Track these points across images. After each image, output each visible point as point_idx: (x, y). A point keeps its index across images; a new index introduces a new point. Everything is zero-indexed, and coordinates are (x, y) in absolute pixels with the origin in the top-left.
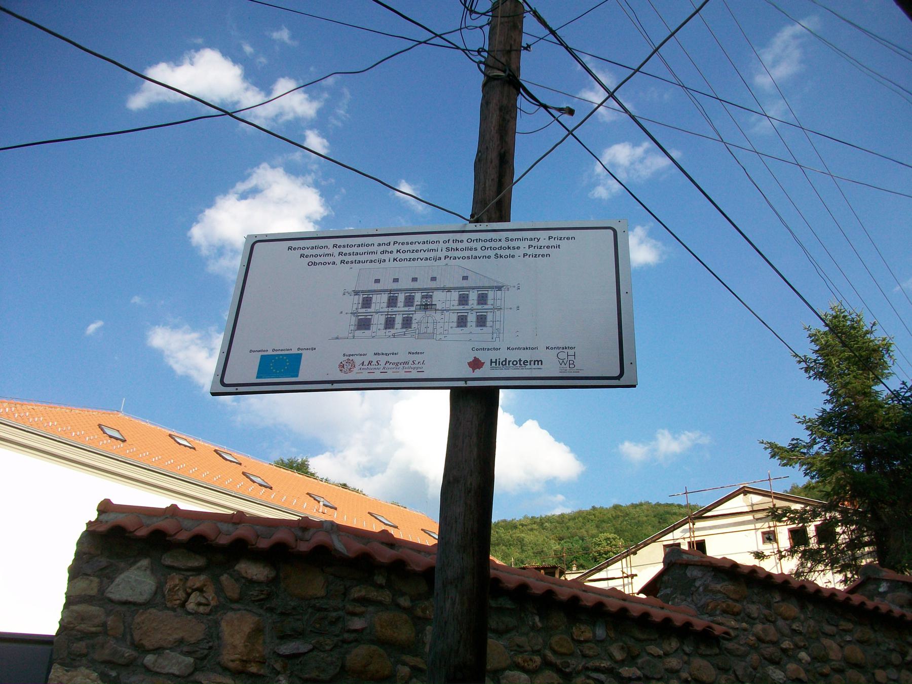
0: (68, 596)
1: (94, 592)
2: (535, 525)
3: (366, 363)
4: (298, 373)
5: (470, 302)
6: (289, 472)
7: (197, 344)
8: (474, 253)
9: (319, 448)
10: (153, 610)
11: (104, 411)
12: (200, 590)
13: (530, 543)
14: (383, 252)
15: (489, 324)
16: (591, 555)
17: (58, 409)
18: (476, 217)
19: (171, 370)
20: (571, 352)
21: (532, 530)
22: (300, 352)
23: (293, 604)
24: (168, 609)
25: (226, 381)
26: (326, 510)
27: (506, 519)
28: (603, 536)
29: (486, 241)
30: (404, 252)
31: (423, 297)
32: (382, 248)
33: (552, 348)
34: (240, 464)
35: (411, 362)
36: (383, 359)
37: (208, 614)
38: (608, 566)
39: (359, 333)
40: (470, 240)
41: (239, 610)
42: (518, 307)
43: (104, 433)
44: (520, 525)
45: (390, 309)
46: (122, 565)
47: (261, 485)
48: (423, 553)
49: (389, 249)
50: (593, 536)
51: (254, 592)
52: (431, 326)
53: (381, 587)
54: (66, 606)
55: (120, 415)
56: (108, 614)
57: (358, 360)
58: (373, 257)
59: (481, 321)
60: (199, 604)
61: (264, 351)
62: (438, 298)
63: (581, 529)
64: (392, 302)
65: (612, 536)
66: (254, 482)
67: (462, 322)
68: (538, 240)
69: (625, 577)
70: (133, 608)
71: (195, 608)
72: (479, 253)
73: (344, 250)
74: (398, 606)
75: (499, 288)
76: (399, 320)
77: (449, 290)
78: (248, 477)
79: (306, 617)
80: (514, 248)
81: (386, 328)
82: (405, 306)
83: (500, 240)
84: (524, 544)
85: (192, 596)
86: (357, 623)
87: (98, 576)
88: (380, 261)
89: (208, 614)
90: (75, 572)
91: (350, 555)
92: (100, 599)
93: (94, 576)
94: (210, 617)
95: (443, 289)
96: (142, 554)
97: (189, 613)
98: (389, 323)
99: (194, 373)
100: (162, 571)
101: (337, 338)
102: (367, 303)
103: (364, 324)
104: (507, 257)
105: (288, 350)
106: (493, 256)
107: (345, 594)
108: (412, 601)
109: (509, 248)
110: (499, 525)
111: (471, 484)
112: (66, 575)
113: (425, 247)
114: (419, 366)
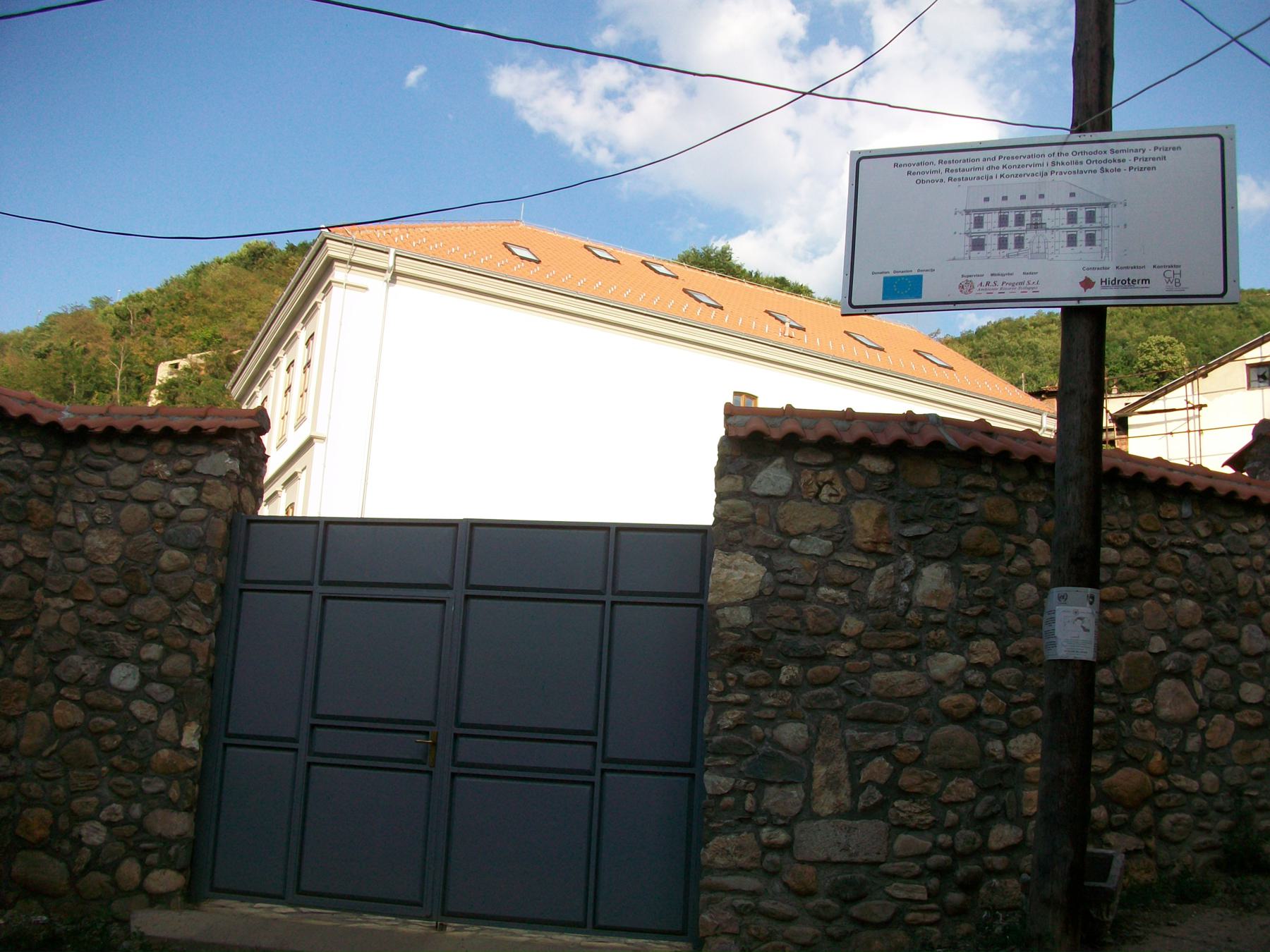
0: (719, 494)
1: (740, 488)
2: (1054, 325)
3: (984, 284)
4: (921, 293)
5: (1079, 221)
6: (736, 282)
7: (558, 87)
8: (1080, 167)
9: (738, 224)
10: (792, 502)
11: (503, 222)
12: (830, 483)
13: (1046, 352)
14: (989, 168)
15: (1098, 243)
16: (1135, 367)
17: (453, 227)
18: (1079, 126)
19: (525, 129)
20: (1177, 271)
21: (1049, 332)
22: (920, 273)
23: (912, 493)
24: (806, 500)
25: (855, 303)
26: (794, 332)
27: (1011, 316)
28: (1154, 339)
29: (1091, 153)
30: (1010, 167)
31: (1033, 216)
32: (989, 163)
33: (1159, 267)
34: (677, 278)
35: (1026, 283)
36: (1000, 280)
37: (840, 504)
38: (1166, 393)
39: (974, 254)
40: (1075, 153)
41: (865, 499)
42: (1125, 225)
43: (514, 253)
44: (1031, 325)
45: (1002, 229)
46: (760, 463)
47: (709, 305)
48: (1018, 440)
49: (995, 164)
50: (1139, 340)
51: (877, 484)
52: (1042, 245)
53: (987, 474)
54: (718, 500)
55: (521, 225)
56: (755, 506)
57: (976, 281)
58: (978, 173)
59: (1090, 240)
60: (831, 495)
61: (886, 273)
62: (1047, 216)
63: (1121, 329)
64: (1003, 221)
65: (1166, 339)
66: (700, 301)
67: (1072, 241)
68: (1144, 151)
69: (1190, 408)
70: (775, 501)
71: (828, 498)
72: (1085, 167)
73: (952, 166)
74: (1003, 491)
75: (1106, 205)
76: (1011, 240)
77: (1058, 207)
78: (691, 296)
79: (924, 504)
80: (1119, 161)
81: (999, 248)
82: (1016, 225)
83: (1105, 152)
84: (1038, 353)
85: (824, 488)
86: (969, 508)
87: (742, 475)
88: (987, 178)
89: (840, 504)
90: (721, 473)
91: (963, 449)
92: (746, 494)
93: (738, 474)
94: (841, 506)
95: (1052, 207)
96: (776, 454)
97: (824, 504)
98: (1003, 244)
99: (557, 129)
100: (796, 468)
101: (954, 259)
102: (979, 222)
103: (978, 245)
104: (1112, 171)
105: (907, 271)
106: (1099, 170)
107: (956, 483)
108: (1014, 486)
109: (1114, 161)
110: (1002, 326)
111: (1086, 395)
112: (713, 475)
113: (1031, 161)
114: (1034, 286)
